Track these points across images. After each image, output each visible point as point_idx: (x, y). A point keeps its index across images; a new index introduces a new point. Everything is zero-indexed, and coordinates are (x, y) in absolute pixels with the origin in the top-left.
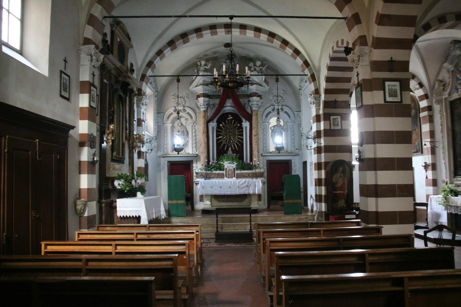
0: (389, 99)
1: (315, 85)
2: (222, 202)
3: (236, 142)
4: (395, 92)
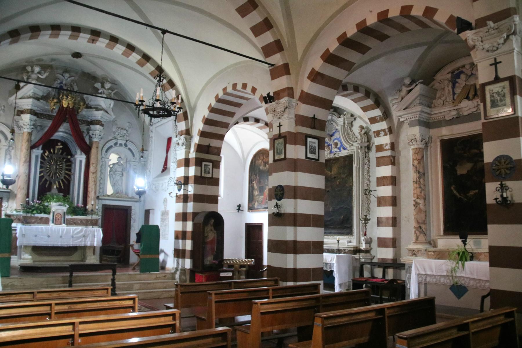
0: (310, 155)
1: (187, 124)
2: (44, 256)
3: (62, 178)
4: (315, 149)
